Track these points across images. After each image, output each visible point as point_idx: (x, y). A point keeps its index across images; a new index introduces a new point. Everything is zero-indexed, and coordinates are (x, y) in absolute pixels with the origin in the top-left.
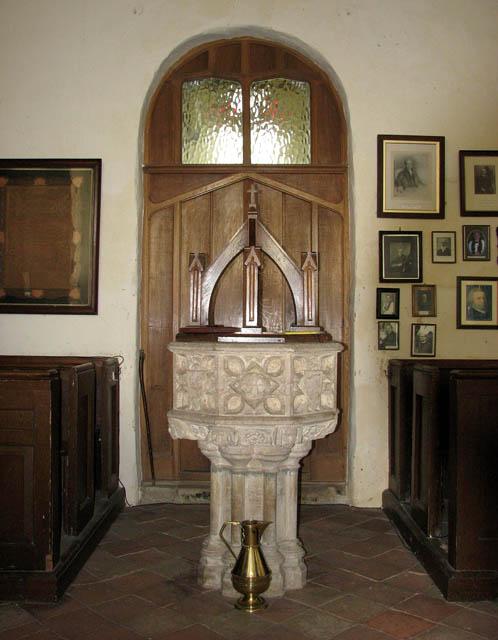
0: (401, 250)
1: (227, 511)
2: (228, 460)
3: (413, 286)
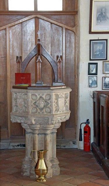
0: (99, 47)
1: (31, 148)
2: (32, 129)
3: (103, 62)
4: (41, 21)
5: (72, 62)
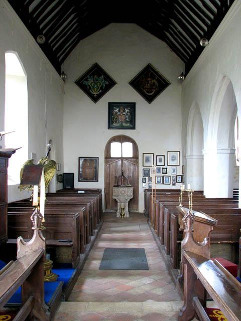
4: (124, 161)
5: (136, 178)
